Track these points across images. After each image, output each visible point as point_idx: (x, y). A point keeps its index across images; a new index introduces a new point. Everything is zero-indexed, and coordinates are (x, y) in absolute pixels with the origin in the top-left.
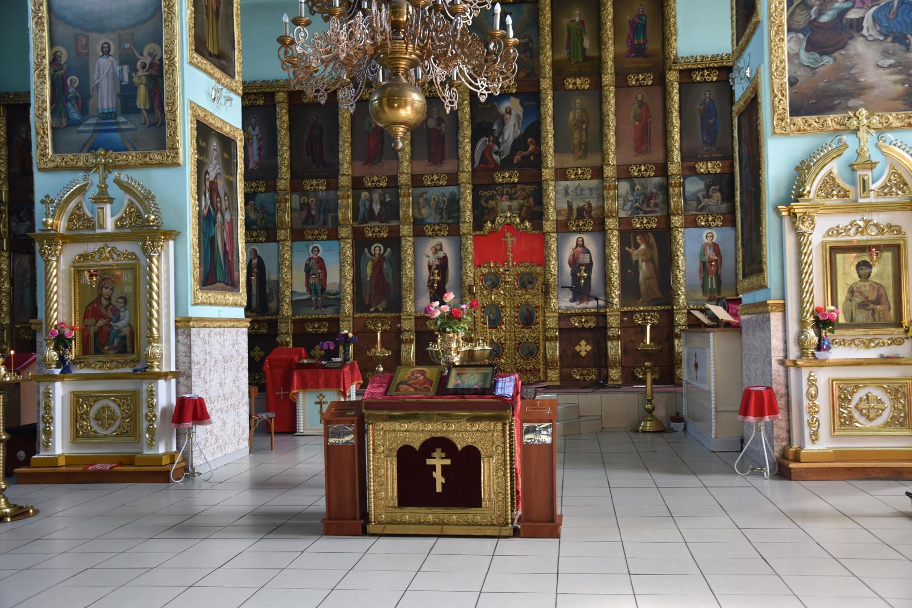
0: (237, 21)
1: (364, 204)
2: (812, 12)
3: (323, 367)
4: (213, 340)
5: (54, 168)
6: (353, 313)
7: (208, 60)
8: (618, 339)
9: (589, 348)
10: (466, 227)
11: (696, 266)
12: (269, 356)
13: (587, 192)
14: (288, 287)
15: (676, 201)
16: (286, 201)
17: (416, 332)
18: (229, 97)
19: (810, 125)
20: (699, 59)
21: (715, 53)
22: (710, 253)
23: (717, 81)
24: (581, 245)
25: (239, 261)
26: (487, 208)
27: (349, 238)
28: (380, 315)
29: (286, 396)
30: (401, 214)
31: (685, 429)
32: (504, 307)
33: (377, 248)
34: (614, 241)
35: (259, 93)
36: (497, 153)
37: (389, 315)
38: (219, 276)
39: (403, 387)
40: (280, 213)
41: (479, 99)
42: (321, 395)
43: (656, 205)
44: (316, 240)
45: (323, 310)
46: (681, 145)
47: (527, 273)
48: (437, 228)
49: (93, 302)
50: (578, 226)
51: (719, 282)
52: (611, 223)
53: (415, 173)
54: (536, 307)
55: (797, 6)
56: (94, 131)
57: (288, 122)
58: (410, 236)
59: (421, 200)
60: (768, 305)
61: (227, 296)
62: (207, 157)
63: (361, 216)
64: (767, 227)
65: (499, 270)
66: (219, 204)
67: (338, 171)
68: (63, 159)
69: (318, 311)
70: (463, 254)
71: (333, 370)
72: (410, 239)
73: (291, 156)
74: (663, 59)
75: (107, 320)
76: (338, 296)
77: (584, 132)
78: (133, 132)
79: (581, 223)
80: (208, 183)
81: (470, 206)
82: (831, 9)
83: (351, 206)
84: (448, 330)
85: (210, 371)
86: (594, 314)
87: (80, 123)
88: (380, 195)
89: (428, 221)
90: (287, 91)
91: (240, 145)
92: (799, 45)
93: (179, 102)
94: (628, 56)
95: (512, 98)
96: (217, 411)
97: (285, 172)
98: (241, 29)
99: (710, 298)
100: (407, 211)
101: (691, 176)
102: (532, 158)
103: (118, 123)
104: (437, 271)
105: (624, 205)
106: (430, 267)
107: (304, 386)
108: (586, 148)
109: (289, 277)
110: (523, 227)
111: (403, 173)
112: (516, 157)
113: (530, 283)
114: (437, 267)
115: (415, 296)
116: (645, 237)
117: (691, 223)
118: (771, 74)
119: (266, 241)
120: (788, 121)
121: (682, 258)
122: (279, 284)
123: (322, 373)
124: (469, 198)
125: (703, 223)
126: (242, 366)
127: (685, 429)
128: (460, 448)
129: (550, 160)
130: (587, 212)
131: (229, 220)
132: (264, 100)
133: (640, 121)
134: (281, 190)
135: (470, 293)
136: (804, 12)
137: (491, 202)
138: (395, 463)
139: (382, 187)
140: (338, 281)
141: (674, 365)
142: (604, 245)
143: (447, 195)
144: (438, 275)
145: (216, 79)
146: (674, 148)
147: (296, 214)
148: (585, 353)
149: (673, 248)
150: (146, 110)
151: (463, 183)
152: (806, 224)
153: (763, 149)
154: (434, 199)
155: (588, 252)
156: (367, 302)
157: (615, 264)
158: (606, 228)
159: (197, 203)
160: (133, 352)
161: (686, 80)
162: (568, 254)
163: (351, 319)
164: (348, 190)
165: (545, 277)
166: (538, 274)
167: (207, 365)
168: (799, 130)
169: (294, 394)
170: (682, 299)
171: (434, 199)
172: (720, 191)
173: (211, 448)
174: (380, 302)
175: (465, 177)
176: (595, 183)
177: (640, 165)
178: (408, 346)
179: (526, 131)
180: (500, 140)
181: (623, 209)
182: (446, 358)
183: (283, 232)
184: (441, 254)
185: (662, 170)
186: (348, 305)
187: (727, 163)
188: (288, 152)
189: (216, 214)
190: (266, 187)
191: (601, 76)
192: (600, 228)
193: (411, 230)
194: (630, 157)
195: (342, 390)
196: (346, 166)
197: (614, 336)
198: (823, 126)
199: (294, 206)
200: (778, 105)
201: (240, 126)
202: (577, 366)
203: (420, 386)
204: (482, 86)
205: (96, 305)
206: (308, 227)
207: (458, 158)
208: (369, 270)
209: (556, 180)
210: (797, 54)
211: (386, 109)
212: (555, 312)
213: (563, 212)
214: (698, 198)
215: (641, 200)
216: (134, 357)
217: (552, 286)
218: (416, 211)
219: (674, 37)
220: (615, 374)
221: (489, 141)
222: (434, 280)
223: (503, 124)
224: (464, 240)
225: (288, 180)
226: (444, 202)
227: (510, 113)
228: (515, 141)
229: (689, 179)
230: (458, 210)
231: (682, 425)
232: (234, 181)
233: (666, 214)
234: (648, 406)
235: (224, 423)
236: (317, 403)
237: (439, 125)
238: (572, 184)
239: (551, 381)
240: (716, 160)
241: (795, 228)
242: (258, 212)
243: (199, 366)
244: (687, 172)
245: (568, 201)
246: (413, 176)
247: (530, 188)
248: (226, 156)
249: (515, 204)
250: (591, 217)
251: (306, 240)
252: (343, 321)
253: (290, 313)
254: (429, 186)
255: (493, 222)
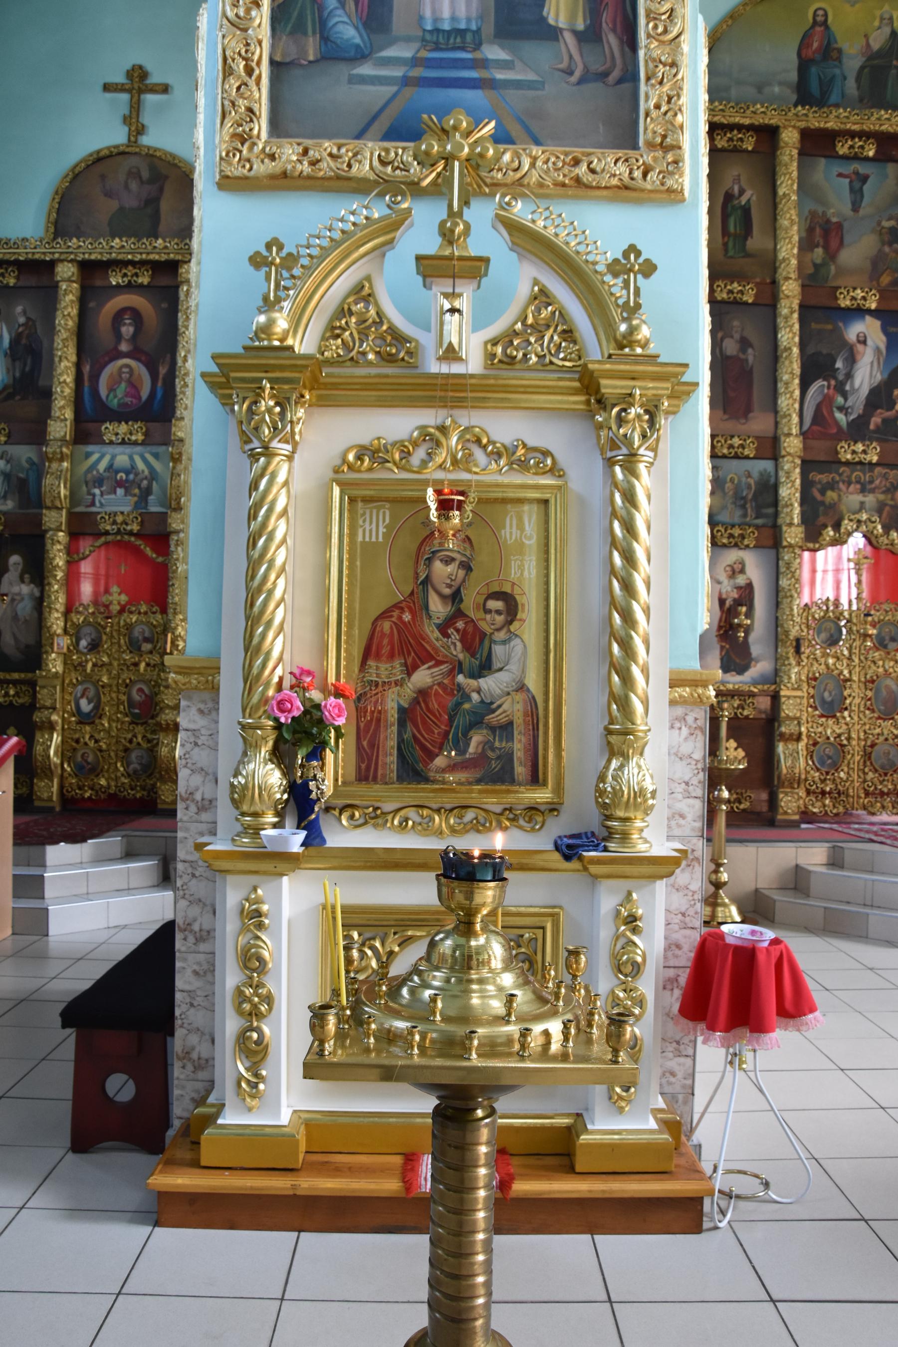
5: (272, 177)
26: (822, 503)
36: (841, 409)
48: (737, 532)
49: (397, 606)
56: (406, 81)
57: (76, 319)
68: (306, 152)
75: (444, 668)
78: (531, 93)
87: (360, 56)
95: (868, 318)
103: (483, 64)
110: (886, 541)
137: (829, 493)
143: (756, 475)
148: (740, 750)
150: (575, 33)
154: (732, 480)
160: (536, 779)
171: (732, 480)
175: (793, 445)
180: (848, 388)
184: (741, 580)
197: (168, 724)
205: (407, 617)
207: (776, 412)
216: (542, 796)
221: (829, 388)
223: (852, 360)
227: (864, 342)
230: (775, 502)
237: (743, 349)
249: (870, 499)
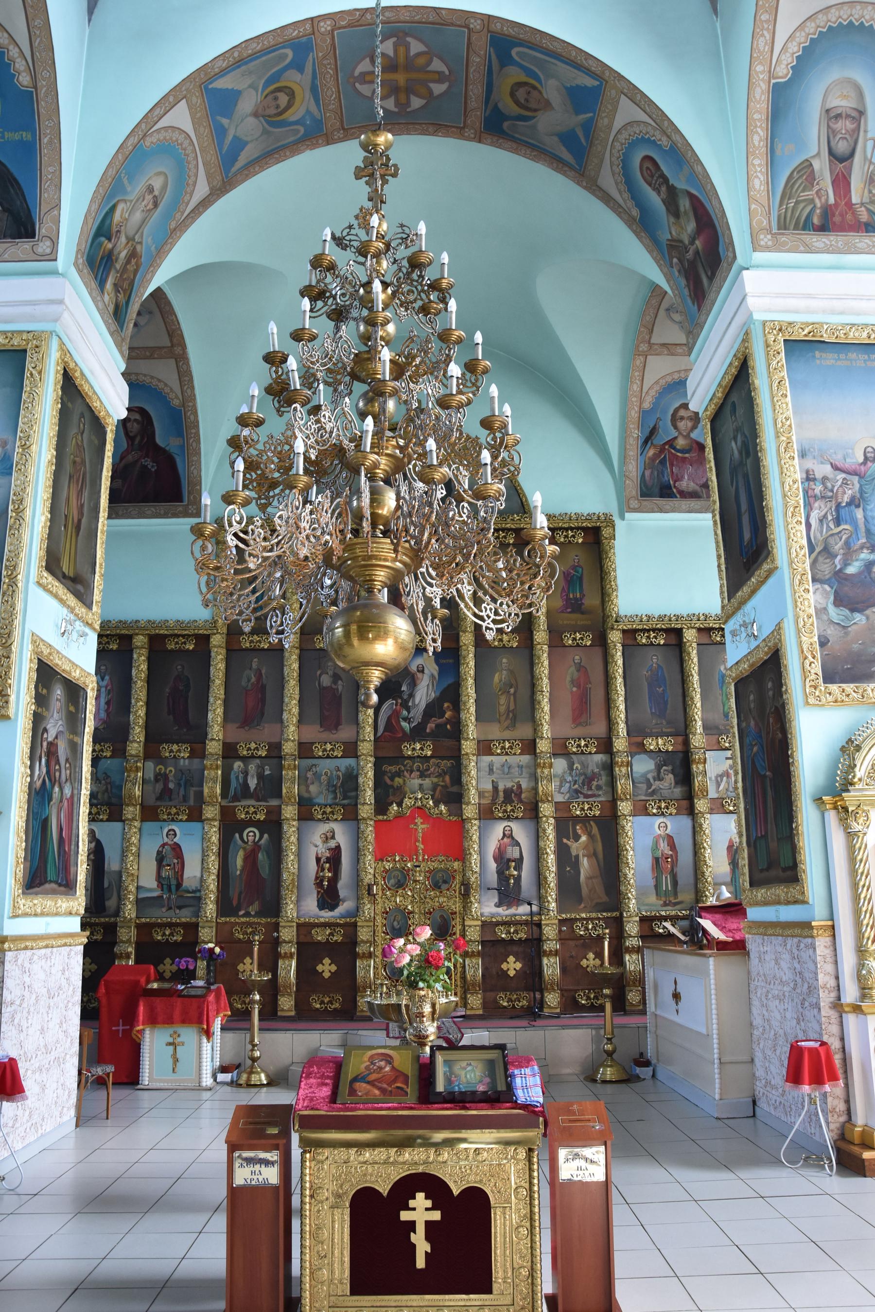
0: (101, 539)
1: (237, 778)
2: (837, 560)
3: (179, 994)
4: (36, 967)
6: (217, 917)
7: (62, 583)
8: (556, 955)
9: (518, 966)
10: (366, 810)
11: (647, 863)
12: (108, 977)
13: (516, 771)
14: (133, 880)
15: (623, 785)
16: (137, 769)
17: (297, 943)
18: (84, 632)
19: (848, 695)
20: (645, 619)
21: (662, 614)
22: (664, 847)
23: (664, 645)
24: (508, 835)
25: (78, 852)
26: (392, 786)
27: (216, 820)
28: (253, 920)
29: (128, 1033)
30: (284, 791)
31: (654, 1076)
32: (411, 912)
33: (251, 834)
34: (550, 831)
35: (113, 636)
36: (405, 719)
37: (264, 920)
38: (51, 874)
39: (362, 1087)
40: (129, 785)
41: (484, 635)
42: (175, 1032)
43: (599, 788)
44: (173, 820)
45: (177, 911)
46: (627, 717)
47: (441, 870)
48: (329, 810)
50: (505, 811)
51: (675, 883)
52: (546, 809)
53: (228, 741)
54: (452, 914)
55: (820, 553)
57: (147, 672)
58: (294, 820)
59: (310, 775)
60: (812, 928)
61: (60, 901)
62: (47, 709)
63: (232, 792)
64: (805, 823)
65: (406, 865)
66: (57, 774)
67: (206, 734)
69: (171, 912)
70: (361, 844)
71: (194, 1000)
72: (294, 823)
73: (147, 714)
74: (603, 617)
76: (198, 894)
77: (512, 698)
79: (509, 808)
80: (45, 744)
81: (371, 784)
82: (857, 560)
83: (220, 779)
84: (421, 985)
85: (29, 1012)
86: (526, 923)
88: (258, 767)
89: (318, 800)
90: (149, 635)
91: (91, 695)
92: (826, 598)
93: (16, 633)
94: (562, 612)
96: (34, 1072)
97: (138, 733)
98: (105, 549)
99: (665, 902)
100: (291, 788)
101: (639, 753)
102: (448, 727)
104: (328, 865)
105: (561, 786)
106: (318, 860)
107: (153, 1021)
108: (515, 717)
109: (136, 867)
110: (437, 812)
111: (288, 740)
112: (429, 725)
113: (445, 882)
114: (328, 860)
115: (298, 896)
116: (586, 827)
117: (642, 810)
118: (798, 631)
119: (108, 820)
120: (823, 689)
121: (632, 852)
122: (121, 877)
123: (178, 1003)
124: (371, 774)
125: (655, 811)
126: (72, 1001)
127: (654, 1076)
128: (456, 1192)
129: (472, 730)
130: (516, 794)
131: (69, 796)
132: (119, 644)
133: (579, 687)
134: (132, 756)
135: (369, 894)
136: (828, 561)
137: (397, 779)
138: (347, 1218)
139: (260, 757)
140: (198, 875)
141: (624, 987)
142: (538, 836)
143: (343, 769)
144: (329, 870)
145: (68, 607)
146: (619, 720)
147: (149, 788)
148: (514, 972)
149: (621, 841)
151: (363, 754)
152: (861, 821)
153: (793, 723)
154: (326, 774)
155: (518, 844)
156: (235, 903)
157: (551, 859)
158: (541, 815)
159: (28, 771)
161: (630, 642)
162: (492, 846)
163: (214, 924)
164: (217, 759)
165: (464, 875)
166: (455, 871)
167: (25, 1005)
168: (836, 701)
169: (138, 1031)
170: (633, 904)
171: (326, 774)
172: (673, 772)
173: (22, 1129)
174: (251, 903)
175: (366, 748)
176: (526, 759)
177: (580, 739)
178: (287, 962)
179: (441, 693)
180: (410, 704)
181: (559, 792)
182: (415, 1029)
183: (131, 809)
184: (332, 844)
185: (606, 746)
186: (211, 906)
187: (680, 739)
188: (144, 709)
189: (53, 787)
190: (113, 751)
191: (532, 632)
192: (533, 814)
193: (296, 812)
194: (568, 730)
195: (205, 1027)
196: (216, 728)
197: (551, 951)
198: (863, 696)
199: (146, 777)
200: (809, 668)
201: (92, 670)
202: (504, 990)
203: (389, 1084)
204: (489, 617)
206: (163, 803)
207: (358, 724)
208: (239, 862)
209: (478, 754)
210: (825, 609)
211: (356, 642)
212: (477, 919)
213: (486, 795)
214: (648, 780)
215: (581, 781)
217: (474, 886)
218: (303, 788)
219: (615, 593)
220: (552, 999)
221: (396, 705)
222: (324, 877)
223: (413, 684)
224: (362, 827)
225: (142, 744)
226: (338, 777)
227: (423, 672)
228: (428, 706)
229: (637, 756)
230: (356, 788)
231: (649, 1070)
232: (79, 742)
233: (610, 799)
234: (609, 1047)
235: (43, 1088)
236: (169, 1044)
237: (335, 682)
238: (498, 761)
239: (472, 1008)
240: (668, 737)
241: (846, 827)
242: (100, 783)
243: (14, 1007)
244: (634, 749)
245: (493, 781)
246: (301, 744)
247: (446, 764)
248: (72, 709)
249: (427, 782)
250: (520, 801)
251: (159, 820)
252: (203, 927)
253: (134, 915)
254: (320, 757)
255: (400, 805)
